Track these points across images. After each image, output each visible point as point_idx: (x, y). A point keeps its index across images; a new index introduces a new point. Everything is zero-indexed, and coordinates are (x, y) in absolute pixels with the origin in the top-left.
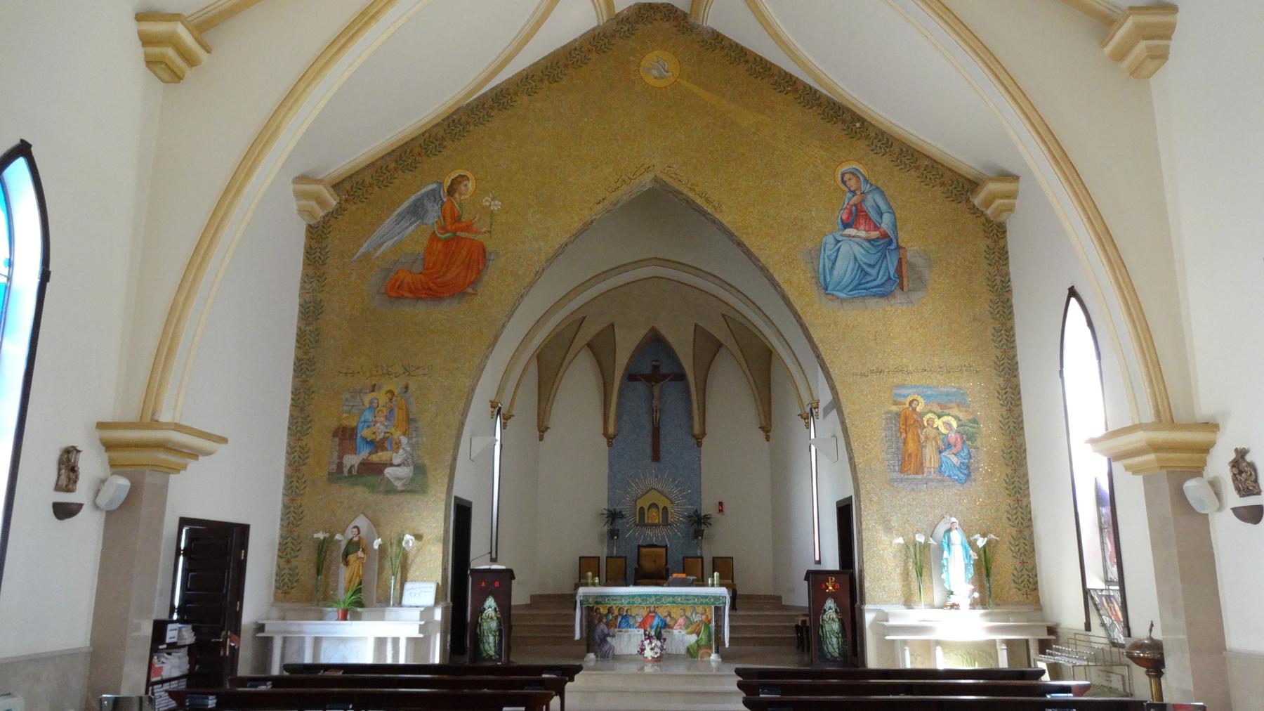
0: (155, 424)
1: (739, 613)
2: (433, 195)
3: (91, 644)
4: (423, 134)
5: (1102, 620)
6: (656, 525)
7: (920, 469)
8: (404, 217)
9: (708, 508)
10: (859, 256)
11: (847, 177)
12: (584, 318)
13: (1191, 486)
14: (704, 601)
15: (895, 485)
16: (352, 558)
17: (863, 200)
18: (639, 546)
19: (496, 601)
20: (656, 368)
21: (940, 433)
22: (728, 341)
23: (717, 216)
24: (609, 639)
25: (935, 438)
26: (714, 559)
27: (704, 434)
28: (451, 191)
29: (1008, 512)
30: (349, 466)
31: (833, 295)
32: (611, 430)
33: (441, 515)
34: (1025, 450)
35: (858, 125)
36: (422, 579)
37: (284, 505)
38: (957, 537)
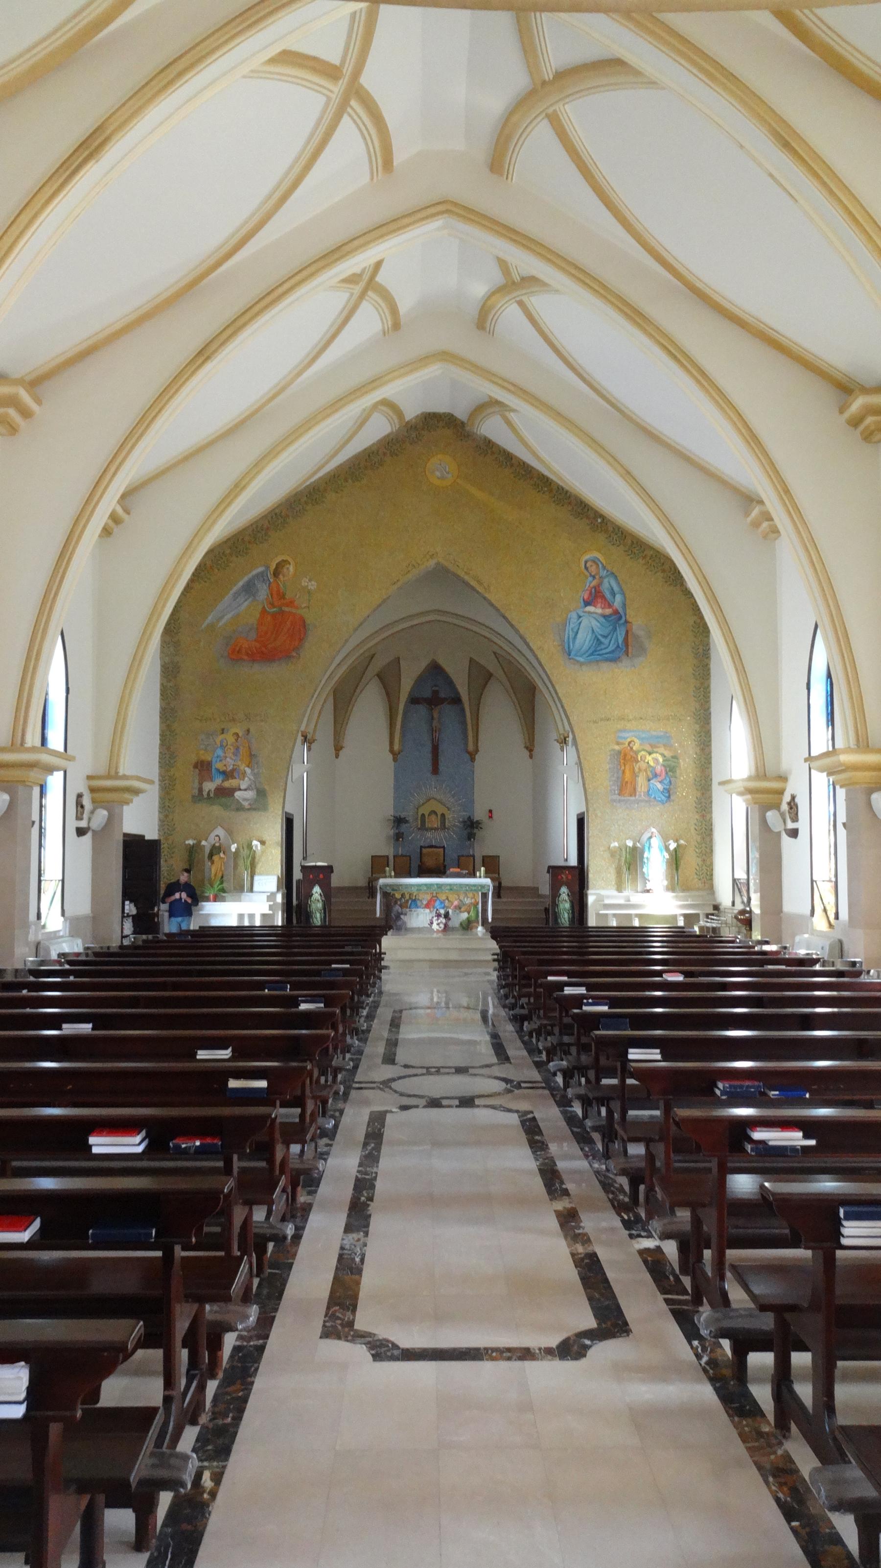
0: (117, 777)
1: (504, 900)
2: (261, 576)
3: (92, 912)
4: (252, 525)
5: (742, 899)
6: (436, 829)
7: (634, 792)
8: (240, 595)
9: (479, 814)
10: (596, 629)
11: (588, 565)
12: (374, 655)
13: (770, 815)
14: (473, 888)
15: (615, 804)
16: (215, 858)
17: (599, 585)
18: (421, 847)
19: (321, 888)
20: (436, 693)
21: (650, 766)
22: (499, 673)
23: (487, 595)
24: (402, 917)
25: (646, 770)
26: (483, 857)
27: (477, 751)
28: (276, 574)
29: (696, 825)
30: (207, 790)
31: (576, 660)
32: (396, 747)
33: (280, 821)
34: (711, 780)
35: (599, 520)
36: (267, 873)
37: (160, 820)
38: (656, 842)
